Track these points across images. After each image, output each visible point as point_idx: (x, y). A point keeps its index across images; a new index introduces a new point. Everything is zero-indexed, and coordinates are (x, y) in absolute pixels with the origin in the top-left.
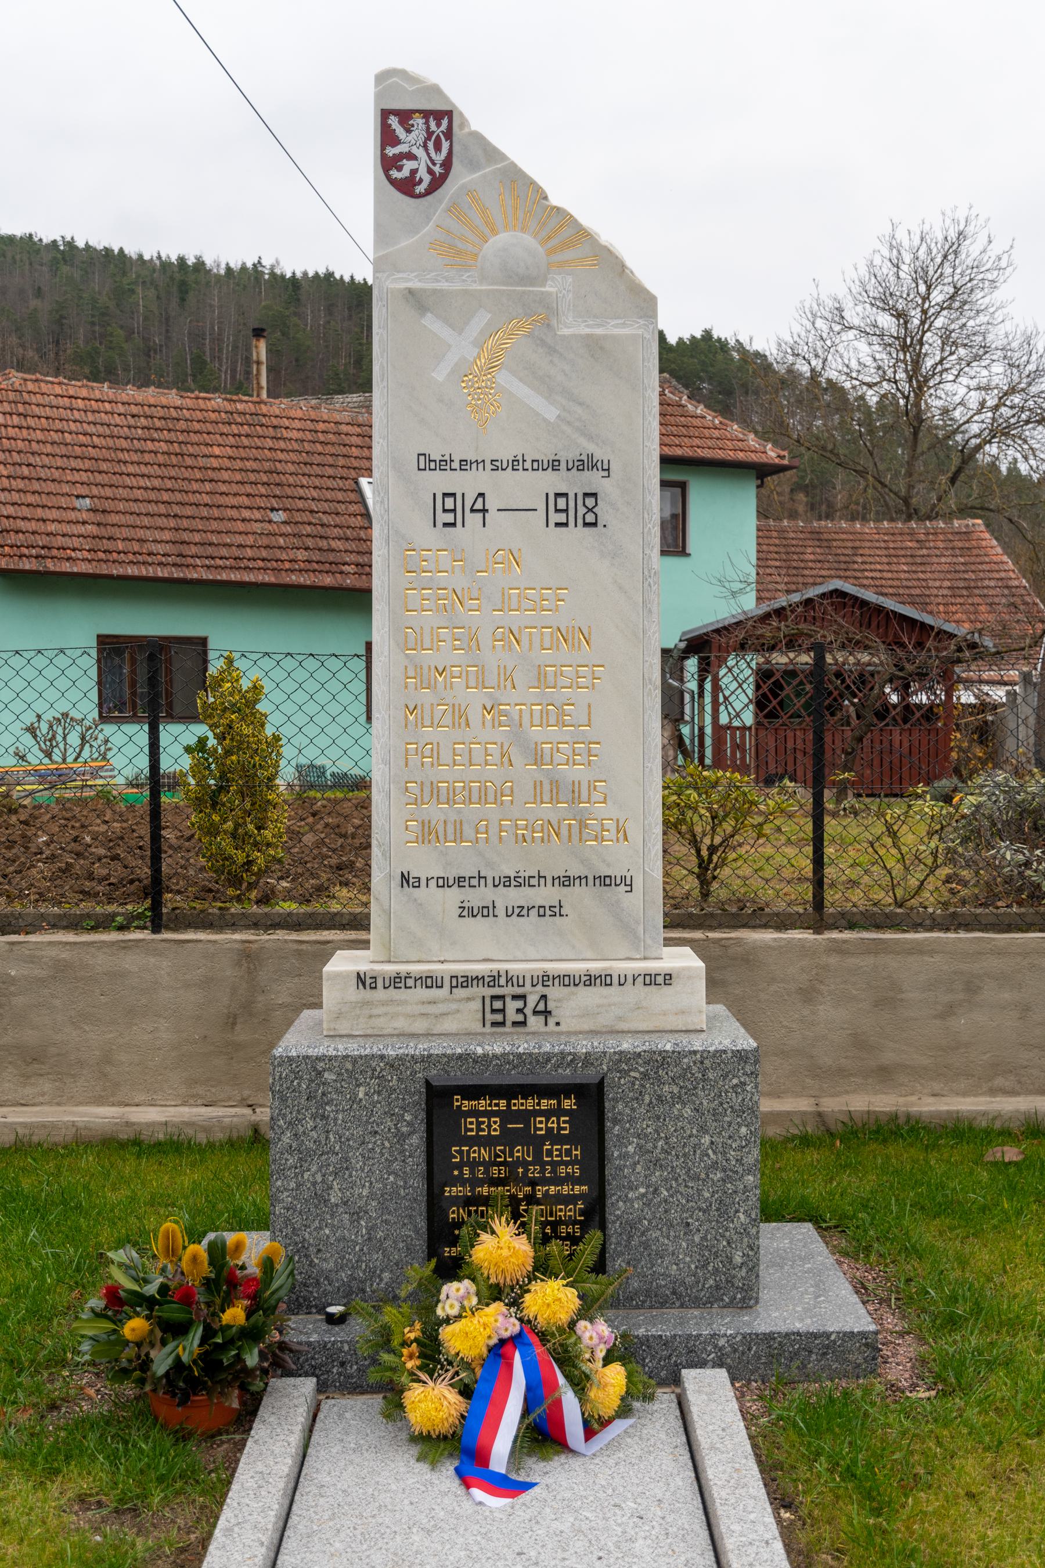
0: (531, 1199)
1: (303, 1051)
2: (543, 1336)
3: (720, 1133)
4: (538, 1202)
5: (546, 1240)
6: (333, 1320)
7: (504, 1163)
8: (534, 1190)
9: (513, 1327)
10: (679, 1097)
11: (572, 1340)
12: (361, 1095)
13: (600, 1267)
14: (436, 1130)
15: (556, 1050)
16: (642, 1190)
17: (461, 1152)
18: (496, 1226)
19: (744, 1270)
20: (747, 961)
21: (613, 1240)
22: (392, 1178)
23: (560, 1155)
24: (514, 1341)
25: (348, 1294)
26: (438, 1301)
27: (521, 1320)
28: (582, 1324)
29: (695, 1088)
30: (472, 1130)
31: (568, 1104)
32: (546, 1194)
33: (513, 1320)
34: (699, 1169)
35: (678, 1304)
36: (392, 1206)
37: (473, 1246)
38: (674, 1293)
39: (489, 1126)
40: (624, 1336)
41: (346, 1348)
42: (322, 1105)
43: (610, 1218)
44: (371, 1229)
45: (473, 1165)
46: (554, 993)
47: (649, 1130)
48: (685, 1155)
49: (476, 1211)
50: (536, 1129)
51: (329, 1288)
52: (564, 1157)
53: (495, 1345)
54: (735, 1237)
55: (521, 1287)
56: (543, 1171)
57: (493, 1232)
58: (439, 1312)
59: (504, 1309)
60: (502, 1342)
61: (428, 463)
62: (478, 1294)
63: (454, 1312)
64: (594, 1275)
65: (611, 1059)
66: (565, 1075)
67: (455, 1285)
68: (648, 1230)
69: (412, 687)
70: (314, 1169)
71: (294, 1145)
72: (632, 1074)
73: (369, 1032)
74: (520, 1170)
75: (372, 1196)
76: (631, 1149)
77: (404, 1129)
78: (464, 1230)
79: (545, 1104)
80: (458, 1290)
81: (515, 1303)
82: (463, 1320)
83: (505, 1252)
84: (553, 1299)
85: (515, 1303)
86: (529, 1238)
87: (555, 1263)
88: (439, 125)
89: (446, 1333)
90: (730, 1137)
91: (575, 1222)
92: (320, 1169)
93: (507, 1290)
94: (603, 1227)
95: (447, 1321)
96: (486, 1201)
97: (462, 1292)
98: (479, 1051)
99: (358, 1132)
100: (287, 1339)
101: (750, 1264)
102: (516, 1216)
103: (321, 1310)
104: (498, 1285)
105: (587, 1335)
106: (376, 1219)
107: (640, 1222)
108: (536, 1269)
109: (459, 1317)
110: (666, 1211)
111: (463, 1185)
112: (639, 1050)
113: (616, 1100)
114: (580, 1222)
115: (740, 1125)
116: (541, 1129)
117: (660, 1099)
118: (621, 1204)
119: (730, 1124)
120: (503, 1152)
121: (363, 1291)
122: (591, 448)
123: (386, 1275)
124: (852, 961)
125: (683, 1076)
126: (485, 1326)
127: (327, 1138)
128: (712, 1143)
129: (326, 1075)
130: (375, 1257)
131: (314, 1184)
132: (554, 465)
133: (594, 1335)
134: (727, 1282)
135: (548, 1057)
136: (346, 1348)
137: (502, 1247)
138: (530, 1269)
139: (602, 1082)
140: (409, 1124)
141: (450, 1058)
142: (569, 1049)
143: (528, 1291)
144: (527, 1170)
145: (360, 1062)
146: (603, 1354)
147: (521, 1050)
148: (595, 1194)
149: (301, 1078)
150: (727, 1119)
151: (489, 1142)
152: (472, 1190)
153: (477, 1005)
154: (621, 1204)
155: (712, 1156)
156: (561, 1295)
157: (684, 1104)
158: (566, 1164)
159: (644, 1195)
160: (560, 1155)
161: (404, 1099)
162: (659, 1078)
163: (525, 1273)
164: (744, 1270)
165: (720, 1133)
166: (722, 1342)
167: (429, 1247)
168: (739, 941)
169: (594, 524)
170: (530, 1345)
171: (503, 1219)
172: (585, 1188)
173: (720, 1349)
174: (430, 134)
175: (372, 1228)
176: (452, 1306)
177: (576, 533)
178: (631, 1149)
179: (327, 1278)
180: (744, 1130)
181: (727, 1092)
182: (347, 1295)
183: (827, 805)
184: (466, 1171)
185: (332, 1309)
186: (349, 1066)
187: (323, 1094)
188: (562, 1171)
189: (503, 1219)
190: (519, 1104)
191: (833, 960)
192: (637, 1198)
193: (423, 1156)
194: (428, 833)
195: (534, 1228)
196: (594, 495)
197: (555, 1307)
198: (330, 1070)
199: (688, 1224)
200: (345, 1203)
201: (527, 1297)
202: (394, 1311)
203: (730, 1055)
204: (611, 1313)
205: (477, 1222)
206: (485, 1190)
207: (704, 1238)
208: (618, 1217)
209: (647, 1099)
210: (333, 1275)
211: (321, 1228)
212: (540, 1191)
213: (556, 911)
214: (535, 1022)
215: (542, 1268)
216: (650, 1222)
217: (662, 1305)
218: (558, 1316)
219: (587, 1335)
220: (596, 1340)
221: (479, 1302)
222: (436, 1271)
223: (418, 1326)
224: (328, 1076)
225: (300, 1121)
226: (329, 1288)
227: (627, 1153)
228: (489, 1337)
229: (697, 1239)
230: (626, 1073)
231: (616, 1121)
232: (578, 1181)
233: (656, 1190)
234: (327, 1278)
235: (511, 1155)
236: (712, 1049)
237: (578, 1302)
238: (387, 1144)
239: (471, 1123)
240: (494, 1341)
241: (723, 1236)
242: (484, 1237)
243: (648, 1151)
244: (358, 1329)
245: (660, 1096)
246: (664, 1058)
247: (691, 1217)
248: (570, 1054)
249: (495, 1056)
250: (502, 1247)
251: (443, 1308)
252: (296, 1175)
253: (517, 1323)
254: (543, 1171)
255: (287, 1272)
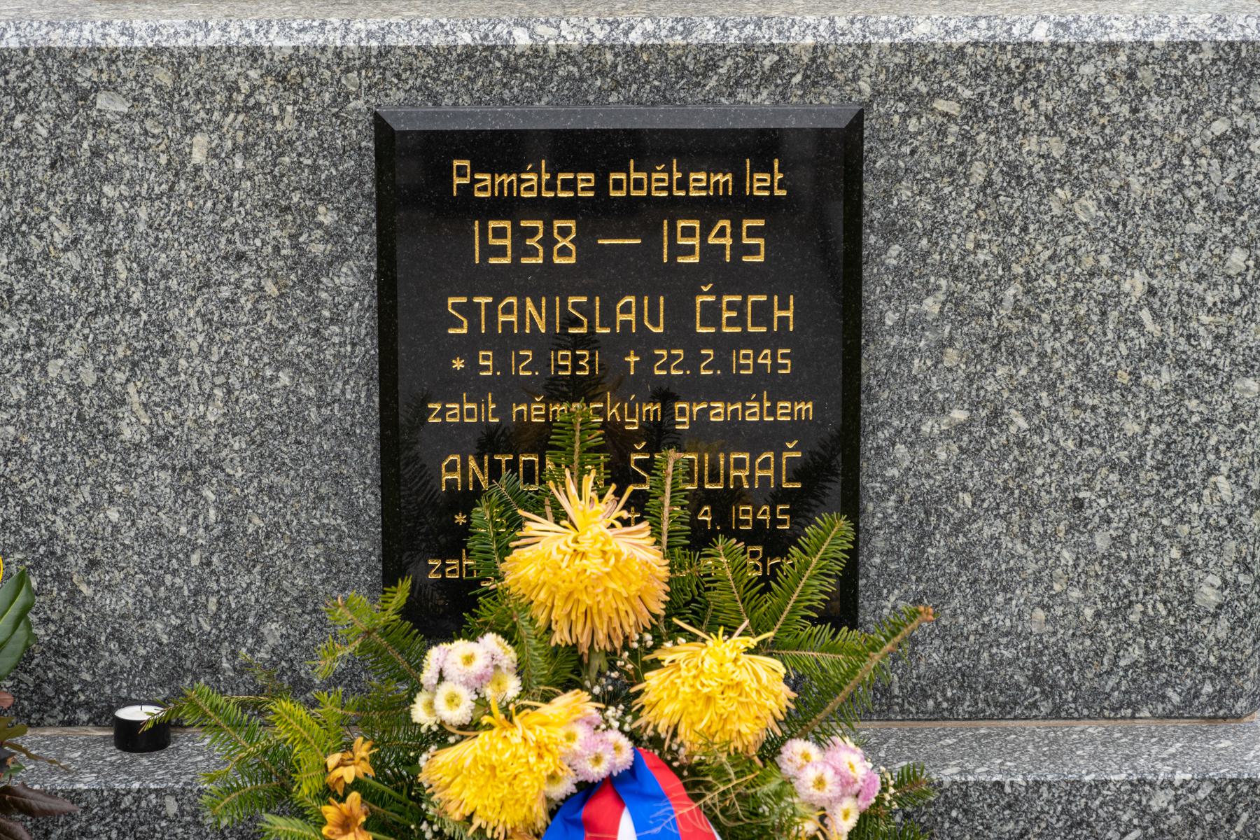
0: (659, 435)
1: (39, 36)
2: (694, 778)
3: (1173, 266)
4: (678, 441)
5: (699, 540)
6: (131, 738)
7: (587, 341)
8: (667, 411)
9: (615, 754)
10: (1067, 170)
11: (772, 786)
12: (198, 157)
13: (842, 610)
14: (403, 253)
15: (733, 38)
16: (959, 415)
17: (470, 310)
18: (572, 506)
19: (1224, 623)
21: (879, 543)
22: (284, 378)
23: (739, 321)
24: (619, 787)
25: (173, 676)
26: (417, 687)
27: (634, 737)
28: (797, 748)
29: (1110, 145)
30: (501, 251)
31: (760, 184)
33: (614, 736)
34: (1113, 360)
35: (1045, 707)
36: (286, 452)
37: (505, 551)
38: (1036, 679)
39: (548, 242)
40: (908, 781)
41: (172, 807)
42: (94, 181)
43: (872, 486)
44: (228, 511)
45: (505, 343)
47: (982, 256)
48: (1076, 323)
49: (513, 465)
50: (676, 250)
51: (121, 659)
52: (756, 324)
53: (568, 798)
54: (1202, 539)
55: (634, 655)
56: (693, 361)
57: (560, 515)
58: (420, 714)
59: (591, 709)
60: (587, 790)
62: (521, 671)
63: (458, 714)
64: (826, 630)
65: (881, 65)
66: (756, 106)
67: (461, 647)
68: (972, 517)
70: (75, 350)
71: (20, 288)
72: (940, 105)
74: (632, 359)
75: (231, 424)
76: (931, 306)
77: (317, 249)
78: (482, 513)
79: (701, 182)
80: (469, 659)
81: (621, 695)
82: (484, 736)
83: (594, 565)
84: (720, 686)
85: (621, 695)
86: (656, 532)
87: (725, 598)
89: (436, 767)
90: (1201, 277)
91: (780, 496)
92: (90, 352)
93: (598, 662)
94: (851, 507)
95: (441, 736)
96: (542, 439)
97: (479, 665)
98: (522, 39)
100: (15, 783)
101: (1242, 608)
102: (619, 476)
103: (103, 714)
104: (573, 648)
105: (810, 775)
106: (245, 484)
107: (951, 495)
108: (673, 609)
109: (471, 727)
110: (1021, 471)
111: (477, 398)
112: (958, 40)
113: (893, 175)
114: (785, 496)
115: (1227, 244)
116: (689, 250)
117: (1013, 172)
118: (901, 449)
119: (1201, 241)
120: (587, 310)
121: (214, 668)
123: (273, 630)
125: (1078, 113)
126: (541, 750)
127: (108, 270)
128: (1152, 291)
129: (102, 101)
130: (243, 581)
133: (829, 775)
134: (1178, 651)
135: (710, 59)
136: (172, 807)
137: (584, 552)
138: (659, 609)
139: (859, 118)
140: (332, 235)
141: (442, 57)
142: (766, 35)
143: (656, 664)
144: (648, 360)
145: (195, 67)
146: (851, 822)
147: (636, 38)
148: (834, 421)
149: (34, 108)
150: (1193, 228)
151: (547, 282)
152: (502, 411)
154: (901, 449)
155: (1150, 326)
156: (742, 675)
157: (1079, 188)
158: (756, 343)
159: (962, 428)
160: (739, 321)
161: (315, 169)
162: (1012, 117)
163: (645, 619)
164: (1224, 623)
165: (1173, 266)
166: (1160, 801)
167: (386, 557)
170: (659, 797)
171: (588, 482)
172: (806, 407)
173: (1155, 819)
175: (233, 508)
176: (452, 700)
178: (931, 306)
179: (115, 635)
180: (1238, 258)
181: (1197, 154)
182: (169, 675)
183: (371, 145)
184: (486, 359)
185: (129, 713)
186: (164, 77)
187: (96, 153)
188: (745, 361)
189: (588, 482)
190: (628, 182)
192: (946, 435)
193: (369, 321)
195: (668, 510)
197: (724, 705)
198: (111, 87)
199: (1079, 504)
200: (161, 442)
201: (653, 679)
202: (301, 712)
203: (1208, 55)
204: (868, 728)
205: (516, 494)
206: (535, 411)
207: (1120, 540)
208: (893, 485)
209: (978, 172)
210: (131, 629)
211: (96, 506)
212: (685, 413)
215: (689, 610)
216: (977, 496)
217: (1004, 711)
218: (732, 726)
219: (810, 775)
220: (832, 788)
221: (525, 691)
222: (406, 612)
223: (362, 749)
224: (110, 104)
225: (33, 223)
226: (121, 659)
227: (920, 317)
228: (552, 778)
229: (1102, 541)
230: (923, 102)
231: (891, 232)
232: (780, 388)
233: (996, 413)
234: (115, 635)
235: (608, 319)
236: (1160, 39)
237: (785, 692)
238: (270, 288)
239: (499, 233)
240: (565, 787)
241: (1172, 536)
242: (536, 526)
243: (979, 313)
244: (202, 763)
245: (1014, 167)
246: (1027, 63)
247: (1088, 485)
248: (770, 48)
249: (564, 54)
250: (584, 552)
251: (430, 705)
252: (27, 368)
253: (626, 743)
254: (693, 361)
255: (13, 612)
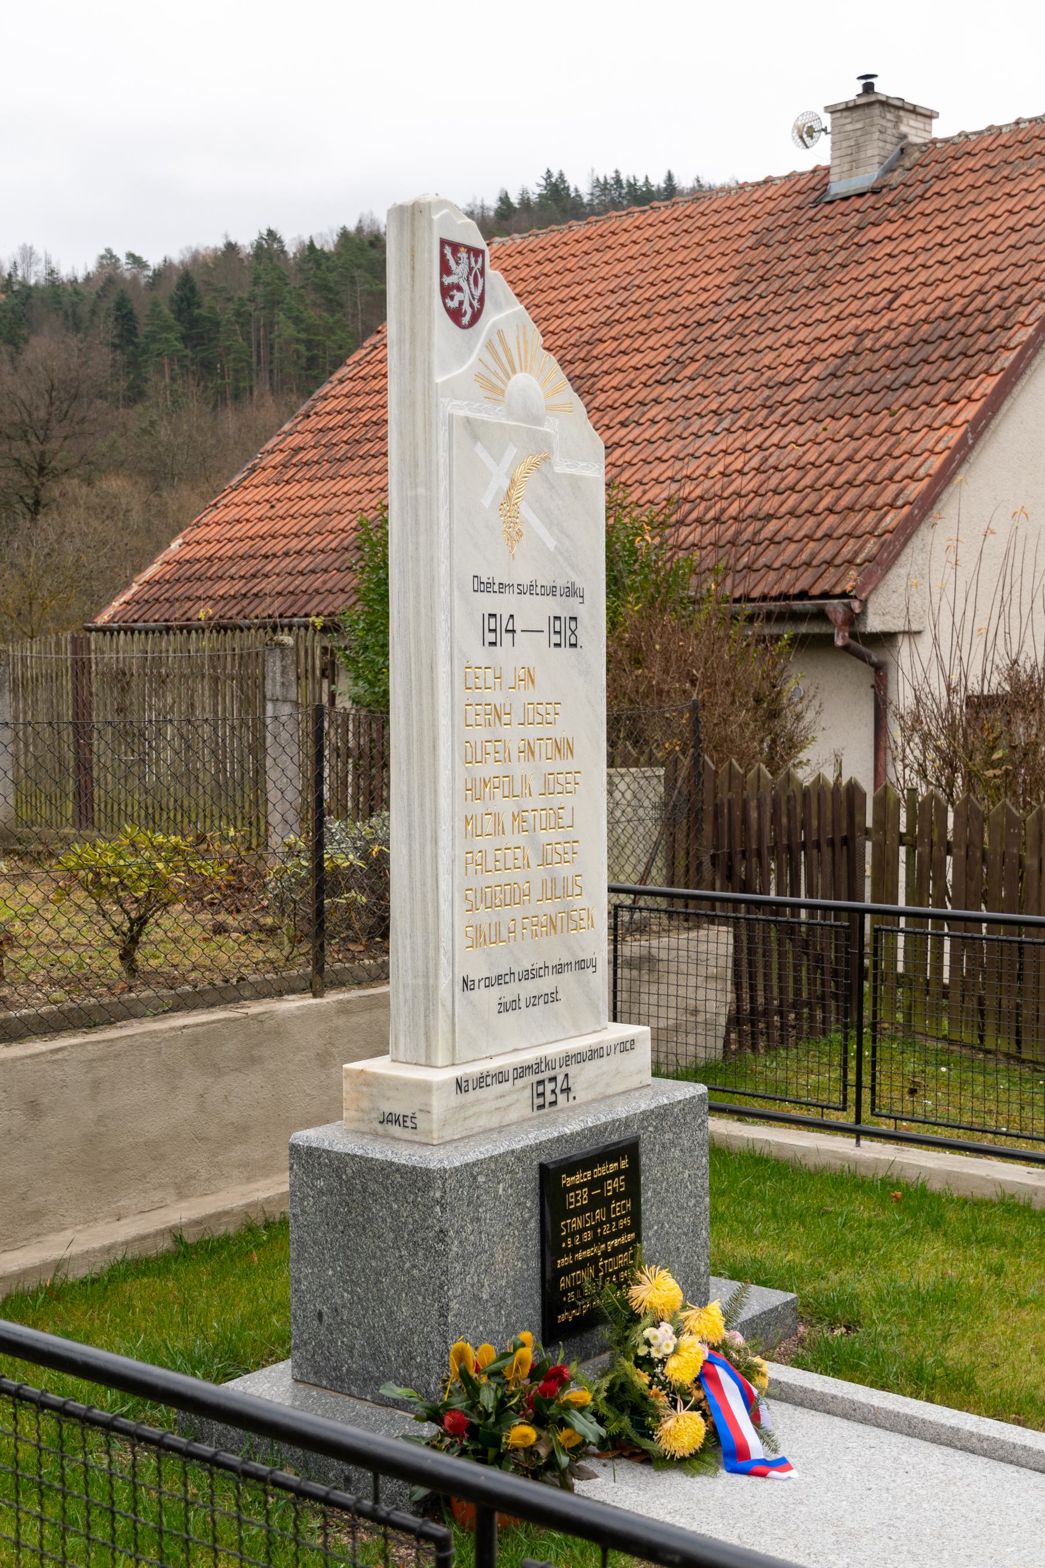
20: (278, 1033)
32: (613, 1247)
46: (573, 1070)
61: (483, 586)
69: (469, 798)
73: (464, 1134)
88: (476, 262)
99: (498, 1227)
122: (574, 577)
124: (355, 1019)
131: (472, 1286)
132: (553, 591)
135: (606, 1125)
153: (528, 1093)
168: (270, 1014)
169: (575, 645)
174: (471, 269)
177: (566, 651)
186: (493, 1166)
191: (340, 1022)
194: (479, 938)
196: (575, 619)
213: (551, 997)
214: (561, 1098)
224: (481, 1179)
